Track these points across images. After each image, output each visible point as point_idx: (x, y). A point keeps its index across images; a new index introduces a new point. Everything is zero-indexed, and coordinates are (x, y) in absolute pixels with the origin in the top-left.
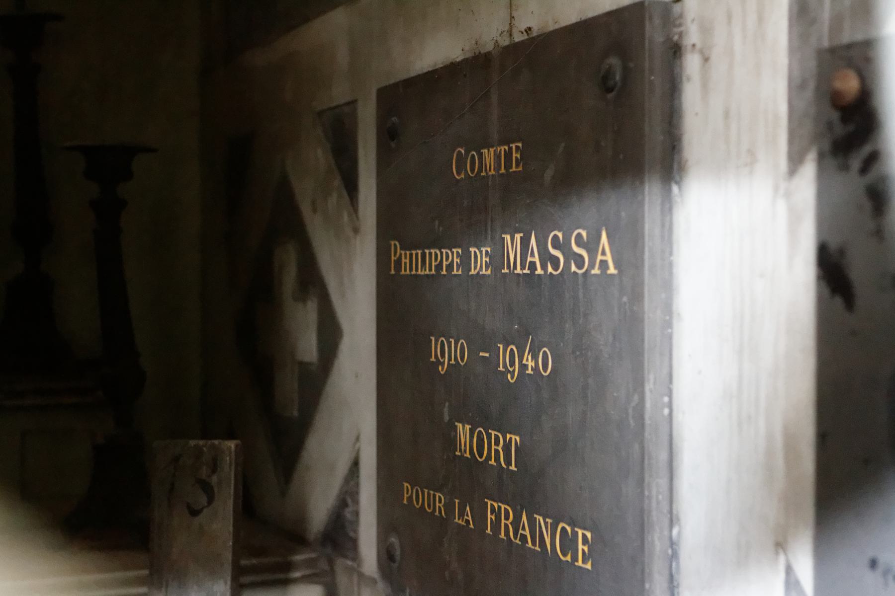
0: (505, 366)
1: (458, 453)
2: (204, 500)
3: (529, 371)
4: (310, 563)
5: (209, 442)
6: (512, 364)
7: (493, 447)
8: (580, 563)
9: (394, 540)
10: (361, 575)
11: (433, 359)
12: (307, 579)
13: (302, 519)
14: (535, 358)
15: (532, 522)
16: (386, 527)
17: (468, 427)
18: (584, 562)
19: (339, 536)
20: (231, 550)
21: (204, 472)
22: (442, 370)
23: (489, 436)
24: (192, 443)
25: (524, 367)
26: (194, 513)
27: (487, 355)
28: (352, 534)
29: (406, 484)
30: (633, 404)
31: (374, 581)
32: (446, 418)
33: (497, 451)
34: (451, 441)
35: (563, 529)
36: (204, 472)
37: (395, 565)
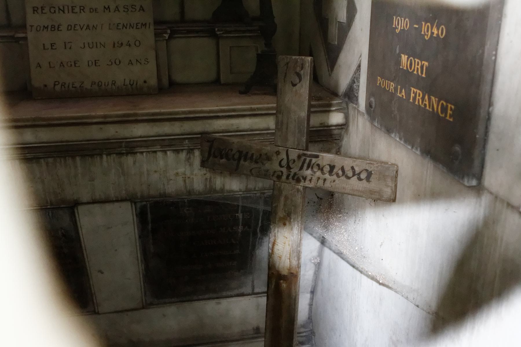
0: (424, 32)
1: (401, 67)
2: (298, 81)
3: (435, 35)
4: (339, 104)
5: (301, 57)
6: (428, 31)
7: (416, 66)
8: (448, 118)
9: (372, 99)
10: (359, 111)
11: (394, 26)
12: (337, 110)
13: (337, 85)
14: (438, 29)
15: (429, 99)
16: (370, 93)
17: (406, 57)
18: (450, 117)
19: (351, 95)
20: (301, 290)
21: (298, 69)
22: (397, 31)
23: (415, 61)
24: (294, 57)
25: (432, 33)
26: (294, 85)
27: (417, 26)
28: (356, 94)
29: (379, 78)
30: (478, 54)
31: (363, 113)
32: (398, 52)
33: (418, 68)
34: (398, 62)
35: (442, 104)
36: (298, 69)
37: (372, 109)
